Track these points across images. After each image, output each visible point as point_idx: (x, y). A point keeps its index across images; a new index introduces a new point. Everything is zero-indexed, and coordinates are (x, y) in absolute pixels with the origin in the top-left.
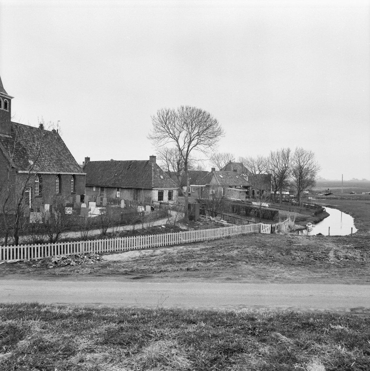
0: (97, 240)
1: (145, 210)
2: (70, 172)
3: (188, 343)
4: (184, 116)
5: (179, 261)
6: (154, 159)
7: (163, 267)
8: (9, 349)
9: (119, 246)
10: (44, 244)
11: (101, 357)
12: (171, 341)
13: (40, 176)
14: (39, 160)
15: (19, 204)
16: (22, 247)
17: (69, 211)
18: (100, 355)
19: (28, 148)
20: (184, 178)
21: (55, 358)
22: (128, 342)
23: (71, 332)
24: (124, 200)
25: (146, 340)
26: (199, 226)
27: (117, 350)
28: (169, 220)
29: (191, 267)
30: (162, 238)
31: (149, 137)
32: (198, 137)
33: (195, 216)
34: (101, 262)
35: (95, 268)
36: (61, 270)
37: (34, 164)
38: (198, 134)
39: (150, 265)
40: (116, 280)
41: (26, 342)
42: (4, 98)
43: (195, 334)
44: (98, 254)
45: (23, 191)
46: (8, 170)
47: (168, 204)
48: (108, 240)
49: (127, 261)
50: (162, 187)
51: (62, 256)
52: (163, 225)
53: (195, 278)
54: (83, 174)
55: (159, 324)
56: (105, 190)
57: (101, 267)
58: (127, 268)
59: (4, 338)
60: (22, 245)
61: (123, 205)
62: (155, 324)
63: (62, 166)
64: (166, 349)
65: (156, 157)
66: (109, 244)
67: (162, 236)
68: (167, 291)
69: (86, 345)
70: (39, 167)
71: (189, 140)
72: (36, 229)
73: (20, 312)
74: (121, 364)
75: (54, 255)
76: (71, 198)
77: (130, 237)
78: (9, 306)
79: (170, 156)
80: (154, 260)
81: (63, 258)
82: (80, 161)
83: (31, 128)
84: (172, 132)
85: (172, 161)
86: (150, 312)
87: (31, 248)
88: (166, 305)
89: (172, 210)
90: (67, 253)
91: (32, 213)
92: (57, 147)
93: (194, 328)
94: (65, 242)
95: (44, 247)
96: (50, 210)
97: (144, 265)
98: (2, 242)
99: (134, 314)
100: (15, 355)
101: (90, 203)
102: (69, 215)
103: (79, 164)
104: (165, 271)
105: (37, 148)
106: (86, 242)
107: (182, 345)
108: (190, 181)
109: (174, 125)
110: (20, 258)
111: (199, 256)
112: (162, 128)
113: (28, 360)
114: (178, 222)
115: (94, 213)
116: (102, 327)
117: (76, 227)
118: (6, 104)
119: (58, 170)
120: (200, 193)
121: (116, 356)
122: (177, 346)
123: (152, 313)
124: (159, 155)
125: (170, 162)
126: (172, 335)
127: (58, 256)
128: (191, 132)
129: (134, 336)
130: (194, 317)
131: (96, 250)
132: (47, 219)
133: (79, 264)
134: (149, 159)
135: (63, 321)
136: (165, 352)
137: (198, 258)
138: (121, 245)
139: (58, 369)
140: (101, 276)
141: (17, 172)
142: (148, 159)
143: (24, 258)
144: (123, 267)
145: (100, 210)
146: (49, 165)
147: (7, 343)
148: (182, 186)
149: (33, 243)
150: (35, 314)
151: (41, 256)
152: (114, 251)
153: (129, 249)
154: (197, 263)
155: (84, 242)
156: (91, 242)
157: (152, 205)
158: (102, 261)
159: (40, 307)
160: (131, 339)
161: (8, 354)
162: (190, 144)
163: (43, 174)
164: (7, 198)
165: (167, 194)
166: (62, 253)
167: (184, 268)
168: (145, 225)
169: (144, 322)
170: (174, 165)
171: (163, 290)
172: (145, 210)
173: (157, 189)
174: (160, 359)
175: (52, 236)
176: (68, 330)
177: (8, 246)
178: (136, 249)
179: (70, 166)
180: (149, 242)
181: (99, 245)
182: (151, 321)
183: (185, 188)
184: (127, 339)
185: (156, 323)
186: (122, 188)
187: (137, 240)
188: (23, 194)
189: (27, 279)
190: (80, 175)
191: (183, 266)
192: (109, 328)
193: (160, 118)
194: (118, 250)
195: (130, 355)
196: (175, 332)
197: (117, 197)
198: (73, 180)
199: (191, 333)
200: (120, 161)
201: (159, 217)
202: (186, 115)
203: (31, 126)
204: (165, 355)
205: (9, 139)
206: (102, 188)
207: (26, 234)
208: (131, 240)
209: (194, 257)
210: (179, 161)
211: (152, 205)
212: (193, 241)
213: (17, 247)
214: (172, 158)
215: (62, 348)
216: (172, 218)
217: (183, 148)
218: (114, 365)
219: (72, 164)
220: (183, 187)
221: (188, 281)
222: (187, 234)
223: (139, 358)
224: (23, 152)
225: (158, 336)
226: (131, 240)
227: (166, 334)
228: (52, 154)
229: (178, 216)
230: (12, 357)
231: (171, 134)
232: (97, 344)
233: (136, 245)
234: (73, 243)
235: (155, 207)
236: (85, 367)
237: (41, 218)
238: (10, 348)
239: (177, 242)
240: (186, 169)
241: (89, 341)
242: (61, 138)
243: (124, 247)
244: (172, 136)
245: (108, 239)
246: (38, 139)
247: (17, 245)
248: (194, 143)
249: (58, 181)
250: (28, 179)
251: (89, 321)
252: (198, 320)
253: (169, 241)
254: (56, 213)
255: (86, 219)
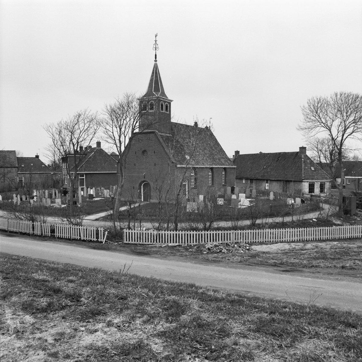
0: (247, 230)
1: (295, 202)
2: (222, 165)
3: (347, 348)
4: (338, 103)
5: (332, 257)
6: (304, 150)
7: (314, 263)
8: (173, 320)
9: (268, 238)
10: (199, 231)
11: (254, 344)
12: (327, 342)
13: (196, 170)
14: (194, 155)
15: (178, 195)
16: (180, 232)
17: (221, 202)
18: (252, 342)
19: (185, 144)
20: (338, 169)
21: (212, 337)
22: (281, 334)
23: (225, 315)
24: (273, 192)
25: (299, 336)
26: (356, 222)
27: (270, 340)
28: (320, 214)
29: (347, 265)
30: (313, 232)
31: (298, 128)
32: (354, 124)
33: (350, 211)
34: (250, 251)
35: (245, 257)
36: (213, 256)
37: (190, 159)
38: (354, 121)
39: (301, 259)
40: (267, 271)
41: (187, 317)
42: (165, 102)
43: (356, 340)
44: (247, 244)
45: (182, 183)
46: (169, 165)
47: (320, 197)
48: (298, 230)
49: (276, 253)
50: (313, 179)
51: (215, 243)
52: (315, 219)
53: (351, 278)
54: (233, 167)
55: (313, 321)
56: (254, 182)
57: (251, 256)
58: (276, 260)
59: (170, 311)
60: (180, 231)
61: (272, 197)
62: (309, 321)
63: (214, 160)
64: (322, 349)
65: (306, 148)
66: (258, 235)
67: (313, 230)
68: (319, 288)
69: (239, 330)
70: (194, 161)
71: (344, 128)
72: (192, 217)
73: (181, 290)
74: (274, 354)
75: (208, 242)
76: (223, 190)
77: (279, 229)
78: (172, 284)
79: (322, 146)
80: (304, 254)
81: (215, 245)
82: (230, 154)
83: (187, 126)
84: (324, 121)
85: (324, 152)
86: (302, 307)
87: (188, 234)
88: (318, 302)
89: (323, 203)
90: (219, 241)
91: (188, 203)
92: (210, 143)
93: (354, 333)
94: (217, 231)
95: (199, 234)
96: (204, 200)
97: (294, 259)
98: (165, 227)
99: (285, 307)
100: (179, 327)
101: (240, 194)
102: (221, 205)
103: (229, 158)
104: (316, 266)
105: (193, 144)
106: (237, 232)
107: (340, 348)
108: (345, 172)
109: (326, 113)
110: (179, 242)
111: (356, 254)
112: (313, 118)
113: (189, 334)
114: (331, 216)
115: (244, 204)
116: (253, 315)
117: (227, 217)
118: (167, 107)
119: (211, 164)
120: (357, 186)
121: (269, 346)
122: (335, 349)
123: (305, 309)
124: (309, 146)
125: (321, 153)
126: (328, 336)
127: (211, 243)
128: (346, 119)
129: (287, 329)
130: (353, 320)
131: (246, 239)
132: (201, 208)
133: (230, 252)
134: (298, 151)
135: (217, 304)
136: (320, 352)
137: (355, 255)
138: (270, 237)
139: (214, 347)
140: (251, 265)
141: (176, 166)
142: (298, 150)
143: (182, 243)
144: (272, 258)
145: (249, 201)
146: (203, 160)
147: (172, 315)
148: (336, 178)
149: (190, 230)
150: (193, 294)
151: (196, 242)
152: (263, 242)
153: (278, 241)
154: (353, 261)
155: (235, 232)
156: (241, 232)
157: (302, 198)
158: (251, 251)
159: (197, 288)
160: (284, 332)
161: (173, 324)
162: (344, 133)
163: (197, 168)
164: (168, 189)
165: (319, 186)
166: (215, 240)
167: (338, 265)
168: (295, 218)
169: (296, 316)
170: (326, 156)
171: (315, 286)
172: (295, 202)
173: (308, 181)
174: (315, 358)
175: (206, 224)
176: (222, 313)
177: (169, 231)
178: (285, 242)
179: (221, 159)
180: (300, 235)
181: (248, 235)
182: (303, 317)
183: (339, 180)
184: (279, 331)
185: (309, 320)
186: (271, 180)
187: (286, 232)
188: (181, 186)
189: (185, 262)
190: (231, 168)
191: (337, 263)
192: (261, 318)
193: (310, 107)
194: (267, 241)
195: (282, 347)
196: (331, 332)
197: (266, 188)
198: (224, 173)
199: (351, 337)
200: (269, 153)
201: (310, 210)
202: (340, 102)
203: (187, 124)
204: (321, 355)
205: (170, 138)
206: (252, 180)
207: (183, 222)
208: (280, 232)
209: (349, 254)
210: (332, 151)
211: (302, 198)
212: (348, 237)
213: (176, 233)
214: (323, 149)
215: (218, 328)
216: (324, 211)
217: (336, 137)
218: (267, 354)
219: (223, 158)
220: (337, 179)
221: (343, 280)
222: (342, 229)
223: (293, 353)
224: (181, 148)
225: (312, 334)
226: (280, 232)
227: (321, 333)
228: (205, 149)
229: (331, 209)
230: (176, 328)
231: (323, 123)
232: (249, 330)
233: (285, 238)
234: (224, 232)
235: (306, 200)
236: (239, 350)
237: (196, 207)
238: (174, 320)
239: (330, 238)
240: (340, 160)
241: (241, 326)
242: (213, 134)
243: (273, 238)
244: (324, 126)
245: (257, 230)
246: (193, 136)
247: (176, 231)
248: (349, 131)
249: (211, 174)
250: (185, 173)
251: (241, 307)
252: (358, 324)
253: (321, 236)
254: (209, 204)
255: (236, 210)
